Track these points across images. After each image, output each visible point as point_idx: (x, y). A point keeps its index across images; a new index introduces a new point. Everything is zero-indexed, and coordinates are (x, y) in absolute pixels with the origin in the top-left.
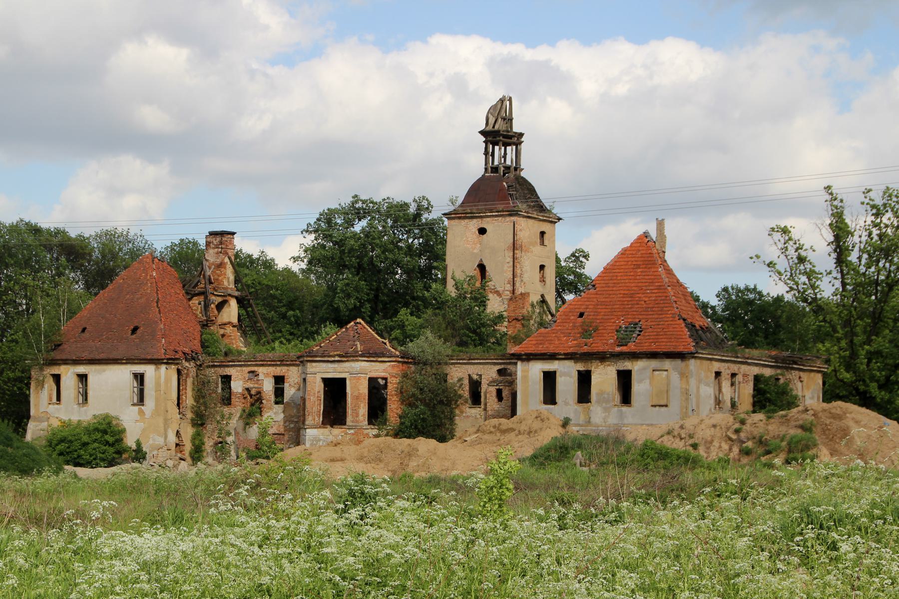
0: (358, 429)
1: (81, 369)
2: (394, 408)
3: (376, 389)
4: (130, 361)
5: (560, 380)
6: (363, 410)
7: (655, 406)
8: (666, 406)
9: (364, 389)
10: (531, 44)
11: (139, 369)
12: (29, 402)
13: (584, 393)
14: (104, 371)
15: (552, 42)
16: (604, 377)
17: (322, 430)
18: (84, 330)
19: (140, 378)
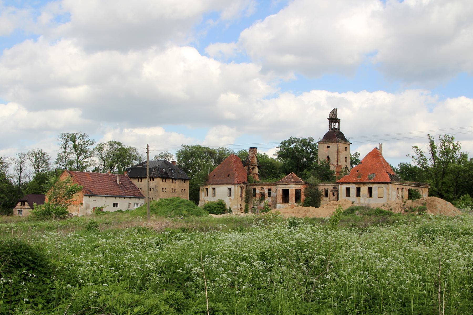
1: (214, 187)
5: (351, 190)
6: (294, 199)
9: (294, 192)
11: (230, 186)
16: (364, 189)
19: (230, 189)
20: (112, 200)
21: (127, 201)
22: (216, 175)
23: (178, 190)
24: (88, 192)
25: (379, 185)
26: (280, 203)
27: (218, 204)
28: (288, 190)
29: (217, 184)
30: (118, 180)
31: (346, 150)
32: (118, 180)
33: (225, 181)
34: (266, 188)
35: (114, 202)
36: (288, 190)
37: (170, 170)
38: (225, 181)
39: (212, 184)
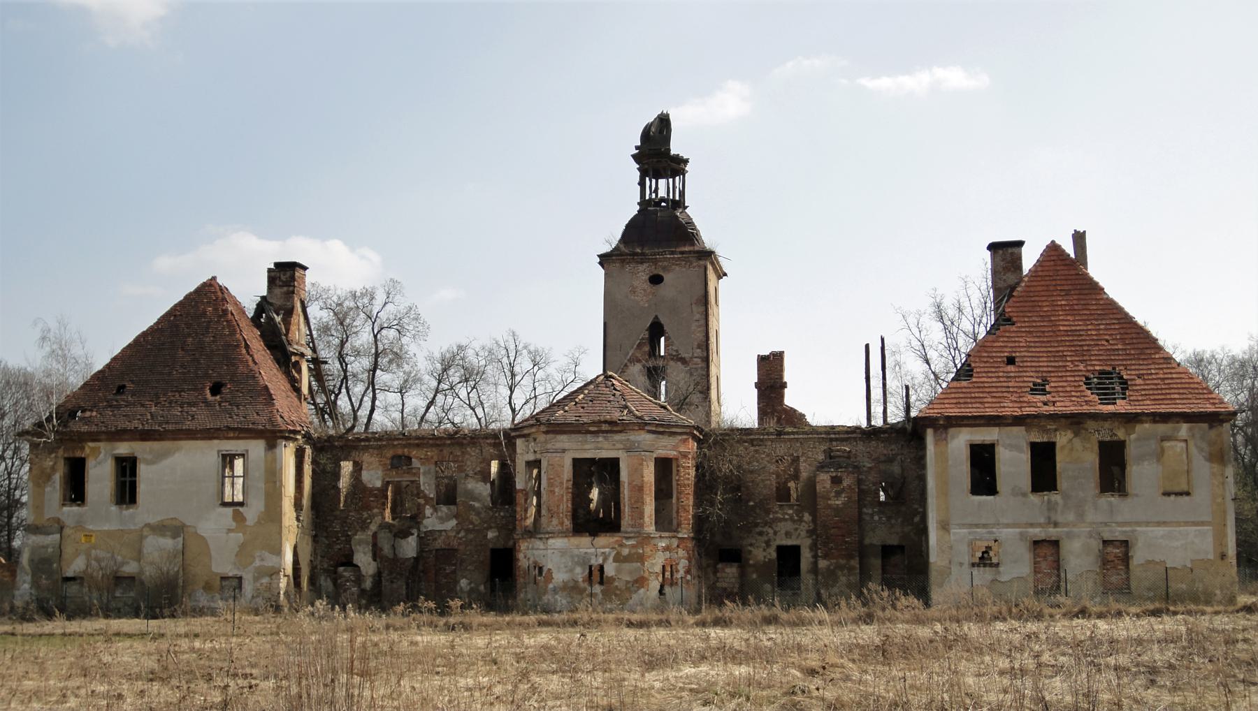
0: (646, 539)
1: (123, 449)
3: (664, 467)
8: (1188, 494)
13: (1044, 472)
16: (1077, 458)
17: (576, 541)
22: (130, 386)
25: (1162, 428)
26: (564, 534)
29: (146, 436)
34: (425, 461)
38: (203, 418)
39: (118, 435)
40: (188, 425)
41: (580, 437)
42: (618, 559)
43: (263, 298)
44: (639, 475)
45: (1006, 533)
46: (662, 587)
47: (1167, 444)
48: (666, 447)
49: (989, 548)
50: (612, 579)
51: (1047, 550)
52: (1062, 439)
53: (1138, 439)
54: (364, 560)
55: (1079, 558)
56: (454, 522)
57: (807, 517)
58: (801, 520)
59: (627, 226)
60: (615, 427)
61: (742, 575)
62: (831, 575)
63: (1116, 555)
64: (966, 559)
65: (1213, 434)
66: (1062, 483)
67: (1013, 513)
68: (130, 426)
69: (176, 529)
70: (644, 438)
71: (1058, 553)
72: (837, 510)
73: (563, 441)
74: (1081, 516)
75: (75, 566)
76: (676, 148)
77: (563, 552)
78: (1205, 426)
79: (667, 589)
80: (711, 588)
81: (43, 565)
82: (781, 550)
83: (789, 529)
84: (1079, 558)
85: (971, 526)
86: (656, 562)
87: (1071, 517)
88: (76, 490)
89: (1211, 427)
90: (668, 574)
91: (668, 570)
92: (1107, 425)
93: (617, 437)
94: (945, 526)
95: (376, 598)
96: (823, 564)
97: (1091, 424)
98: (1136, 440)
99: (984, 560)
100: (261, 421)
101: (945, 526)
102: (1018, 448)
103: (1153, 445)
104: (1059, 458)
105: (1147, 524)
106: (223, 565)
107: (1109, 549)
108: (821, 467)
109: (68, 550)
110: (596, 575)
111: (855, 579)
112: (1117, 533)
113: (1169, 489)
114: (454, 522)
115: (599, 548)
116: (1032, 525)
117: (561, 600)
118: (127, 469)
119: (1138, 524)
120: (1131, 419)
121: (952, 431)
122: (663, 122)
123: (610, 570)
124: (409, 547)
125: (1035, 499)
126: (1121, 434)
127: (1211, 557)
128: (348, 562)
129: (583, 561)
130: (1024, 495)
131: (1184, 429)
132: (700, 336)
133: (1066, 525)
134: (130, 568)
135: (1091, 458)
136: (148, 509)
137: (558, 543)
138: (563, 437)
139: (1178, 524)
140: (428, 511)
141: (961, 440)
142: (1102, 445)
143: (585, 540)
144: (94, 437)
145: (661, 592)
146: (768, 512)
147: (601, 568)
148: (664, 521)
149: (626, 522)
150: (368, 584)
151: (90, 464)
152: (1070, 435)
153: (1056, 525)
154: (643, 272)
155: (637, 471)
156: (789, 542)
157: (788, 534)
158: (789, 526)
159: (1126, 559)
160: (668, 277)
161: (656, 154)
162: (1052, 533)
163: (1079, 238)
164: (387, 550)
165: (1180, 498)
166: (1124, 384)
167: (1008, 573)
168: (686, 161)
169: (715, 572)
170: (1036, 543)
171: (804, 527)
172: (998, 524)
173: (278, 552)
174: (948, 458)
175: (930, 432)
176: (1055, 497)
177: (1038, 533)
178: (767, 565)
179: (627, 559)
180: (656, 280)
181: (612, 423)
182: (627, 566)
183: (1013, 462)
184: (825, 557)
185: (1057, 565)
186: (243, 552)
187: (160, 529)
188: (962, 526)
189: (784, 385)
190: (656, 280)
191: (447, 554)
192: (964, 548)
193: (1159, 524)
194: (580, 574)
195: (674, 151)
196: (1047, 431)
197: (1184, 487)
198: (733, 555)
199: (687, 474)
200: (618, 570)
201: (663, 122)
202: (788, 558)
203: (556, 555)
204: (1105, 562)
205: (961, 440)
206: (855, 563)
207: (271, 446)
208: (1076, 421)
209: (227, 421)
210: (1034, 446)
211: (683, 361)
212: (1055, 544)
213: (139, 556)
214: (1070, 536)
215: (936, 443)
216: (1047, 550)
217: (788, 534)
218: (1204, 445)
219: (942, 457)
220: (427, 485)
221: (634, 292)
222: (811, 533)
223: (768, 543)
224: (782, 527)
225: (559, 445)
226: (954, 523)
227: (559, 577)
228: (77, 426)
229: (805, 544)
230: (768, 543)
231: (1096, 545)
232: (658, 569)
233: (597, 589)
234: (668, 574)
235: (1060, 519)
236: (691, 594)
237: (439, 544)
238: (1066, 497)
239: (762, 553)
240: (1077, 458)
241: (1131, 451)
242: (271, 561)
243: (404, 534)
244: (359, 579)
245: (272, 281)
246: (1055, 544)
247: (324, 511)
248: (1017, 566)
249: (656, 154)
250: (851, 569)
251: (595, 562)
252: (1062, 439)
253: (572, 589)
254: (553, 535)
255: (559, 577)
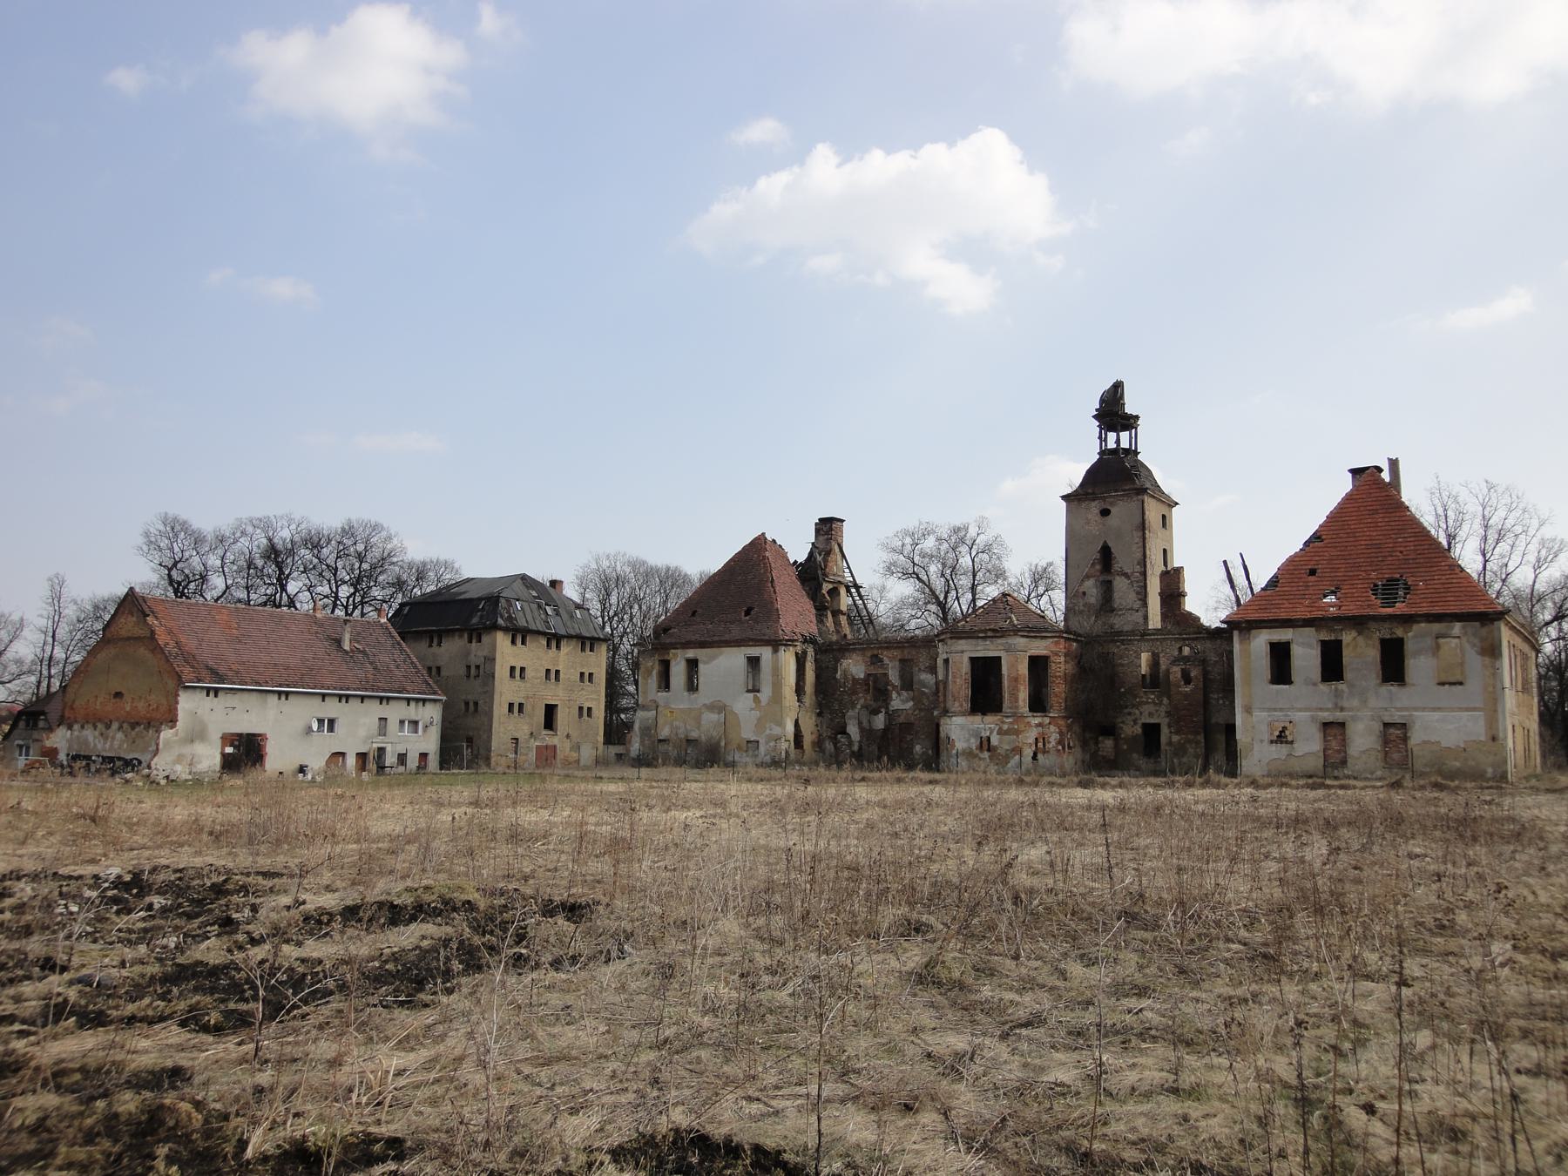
0: (1018, 717)
1: (691, 654)
2: (1058, 690)
3: (1038, 665)
4: (739, 643)
5: (1297, 651)
6: (1023, 695)
7: (1443, 684)
8: (1461, 684)
9: (1023, 669)
10: (850, 148)
11: (754, 651)
12: (1233, 691)
13: (1332, 667)
14: (713, 658)
15: (915, 146)
16: (1361, 653)
17: (971, 718)
18: (694, 613)
19: (754, 662)
20: (304, 711)
21: (375, 710)
22: (700, 611)
23: (570, 674)
24: (204, 673)
25: (1437, 627)
26: (963, 714)
27: (819, 715)
28: (997, 661)
29: (702, 645)
30: (347, 637)
31: (1164, 525)
32: (347, 637)
33: (736, 632)
34: (892, 659)
35: (321, 716)
36: (997, 661)
37: (540, 606)
38: (736, 632)
39: (687, 645)
40: (727, 637)
41: (973, 641)
42: (999, 733)
43: (131, 603)
44: (1015, 669)
45: (1299, 716)
46: (1035, 754)
47: (1442, 641)
48: (1040, 648)
49: (1284, 728)
50: (995, 748)
51: (1334, 729)
52: (1347, 637)
53: (1415, 637)
54: (853, 729)
55: (1363, 740)
56: (911, 704)
57: (1165, 701)
58: (1161, 703)
59: (1089, 472)
60: (998, 633)
61: (1116, 746)
62: (1180, 750)
63: (1394, 734)
64: (1266, 737)
65: (1484, 631)
66: (1348, 674)
67: (1304, 703)
68: (693, 638)
69: (719, 707)
70: (1020, 642)
71: (1344, 734)
72: (1186, 695)
73: (962, 644)
74: (1364, 702)
75: (665, 732)
76: (1129, 409)
77: (962, 727)
78: (1477, 624)
79: (1040, 756)
80: (1094, 755)
81: (646, 731)
82: (1145, 726)
83: (1151, 710)
84: (1363, 740)
85: (1269, 710)
86: (1030, 736)
87: (1355, 703)
88: (665, 683)
89: (1483, 625)
90: (1040, 745)
91: (1042, 739)
92: (1387, 625)
93: (999, 641)
94: (1248, 710)
95: (861, 758)
96: (1175, 738)
97: (1373, 625)
98: (1415, 639)
99: (1281, 738)
100: (768, 634)
101: (1248, 710)
102: (1310, 646)
103: (1429, 641)
104: (1345, 652)
105: (1424, 709)
106: (748, 733)
107: (1392, 730)
108: (1175, 662)
109: (661, 721)
110: (985, 744)
111: (1201, 751)
112: (1396, 718)
113: (1443, 679)
114: (911, 704)
115: (986, 724)
116: (1321, 709)
117: (963, 763)
118: (693, 664)
119: (1416, 709)
120: (1408, 620)
121: (1254, 632)
122: (1118, 387)
123: (995, 741)
124: (880, 721)
125: (1323, 687)
126: (1399, 632)
127: (1483, 738)
128: (844, 732)
129: (976, 733)
130: (1315, 684)
131: (1457, 628)
132: (1139, 555)
133: (1351, 710)
134: (694, 735)
135: (1373, 654)
136: (705, 695)
137: (958, 720)
138: (962, 642)
139: (1452, 710)
140: (894, 695)
141: (1261, 641)
142: (1383, 642)
143: (978, 718)
144: (674, 646)
145: (1035, 757)
146: (1136, 696)
147: (989, 739)
148: (1038, 704)
149: (1006, 704)
150: (856, 748)
151: (672, 664)
152: (1354, 634)
153: (1342, 709)
154: (1095, 507)
155: (1013, 666)
156: (1152, 721)
157: (1151, 714)
158: (1151, 708)
159: (1405, 739)
160: (1113, 510)
161: (1113, 413)
162: (1339, 716)
163: (1394, 464)
164: (865, 724)
165: (1453, 688)
166: (1408, 588)
167: (1301, 748)
168: (1137, 417)
169: (1097, 743)
170: (1326, 725)
171: (1163, 709)
172: (1292, 709)
173: (781, 724)
174: (1253, 652)
175: (1236, 633)
176: (1341, 686)
177: (1327, 716)
178: (1135, 738)
179: (1007, 733)
180: (1105, 513)
181: (993, 630)
182: (1007, 738)
183: (1306, 655)
184: (1177, 733)
185: (1344, 743)
186: (760, 725)
187: (712, 707)
188: (1263, 710)
189: (1183, 595)
190: (1105, 513)
191: (907, 727)
192: (1264, 728)
193: (1434, 709)
194: (974, 743)
195: (1129, 410)
196: (1334, 631)
197: (1459, 678)
198: (1110, 731)
199: (1060, 667)
200: (1001, 741)
201: (1118, 387)
202: (1152, 731)
203: (960, 729)
204: (1386, 741)
205: (1261, 641)
206: (1201, 738)
207: (776, 651)
208: (1359, 622)
209: (750, 634)
210: (1323, 643)
211: (1126, 575)
212: (1342, 725)
213: (699, 726)
214: (1354, 719)
215: (1241, 642)
216: (1334, 729)
217: (1151, 714)
218: (1476, 641)
219: (1246, 654)
220: (894, 676)
221: (1088, 523)
222: (1168, 714)
223: (1135, 721)
224: (1147, 709)
225: (959, 648)
226: (1257, 711)
227: (960, 745)
228: (665, 639)
229: (1164, 722)
230: (1135, 721)
231: (1378, 727)
232: (1031, 740)
233: (986, 755)
234: (1040, 745)
235: (1346, 704)
236: (1069, 761)
237: (902, 719)
238: (1351, 686)
239: (1131, 729)
240: (1361, 653)
241: (1409, 646)
242: (777, 731)
243: (876, 712)
244: (851, 743)
245: (818, 531)
246: (1342, 725)
247: (828, 695)
248: (1309, 745)
249: (1113, 413)
250: (1197, 743)
251: (985, 734)
252: (1347, 637)
253: (969, 754)
254: (956, 714)
255: (960, 745)
